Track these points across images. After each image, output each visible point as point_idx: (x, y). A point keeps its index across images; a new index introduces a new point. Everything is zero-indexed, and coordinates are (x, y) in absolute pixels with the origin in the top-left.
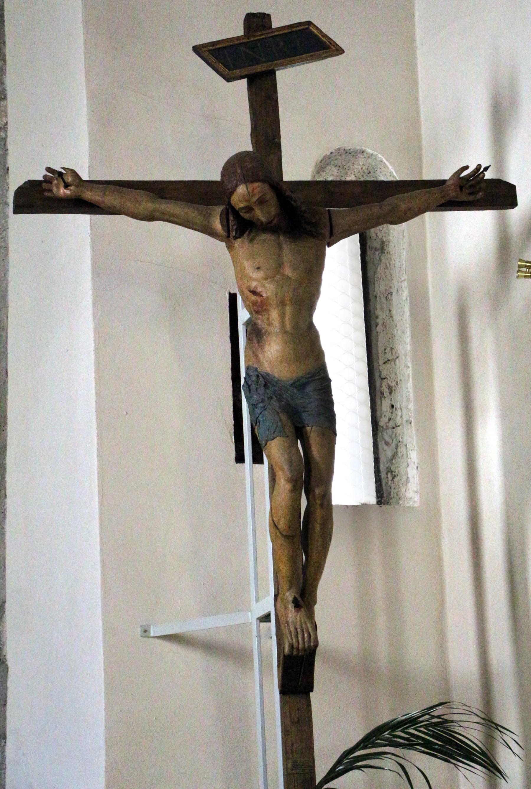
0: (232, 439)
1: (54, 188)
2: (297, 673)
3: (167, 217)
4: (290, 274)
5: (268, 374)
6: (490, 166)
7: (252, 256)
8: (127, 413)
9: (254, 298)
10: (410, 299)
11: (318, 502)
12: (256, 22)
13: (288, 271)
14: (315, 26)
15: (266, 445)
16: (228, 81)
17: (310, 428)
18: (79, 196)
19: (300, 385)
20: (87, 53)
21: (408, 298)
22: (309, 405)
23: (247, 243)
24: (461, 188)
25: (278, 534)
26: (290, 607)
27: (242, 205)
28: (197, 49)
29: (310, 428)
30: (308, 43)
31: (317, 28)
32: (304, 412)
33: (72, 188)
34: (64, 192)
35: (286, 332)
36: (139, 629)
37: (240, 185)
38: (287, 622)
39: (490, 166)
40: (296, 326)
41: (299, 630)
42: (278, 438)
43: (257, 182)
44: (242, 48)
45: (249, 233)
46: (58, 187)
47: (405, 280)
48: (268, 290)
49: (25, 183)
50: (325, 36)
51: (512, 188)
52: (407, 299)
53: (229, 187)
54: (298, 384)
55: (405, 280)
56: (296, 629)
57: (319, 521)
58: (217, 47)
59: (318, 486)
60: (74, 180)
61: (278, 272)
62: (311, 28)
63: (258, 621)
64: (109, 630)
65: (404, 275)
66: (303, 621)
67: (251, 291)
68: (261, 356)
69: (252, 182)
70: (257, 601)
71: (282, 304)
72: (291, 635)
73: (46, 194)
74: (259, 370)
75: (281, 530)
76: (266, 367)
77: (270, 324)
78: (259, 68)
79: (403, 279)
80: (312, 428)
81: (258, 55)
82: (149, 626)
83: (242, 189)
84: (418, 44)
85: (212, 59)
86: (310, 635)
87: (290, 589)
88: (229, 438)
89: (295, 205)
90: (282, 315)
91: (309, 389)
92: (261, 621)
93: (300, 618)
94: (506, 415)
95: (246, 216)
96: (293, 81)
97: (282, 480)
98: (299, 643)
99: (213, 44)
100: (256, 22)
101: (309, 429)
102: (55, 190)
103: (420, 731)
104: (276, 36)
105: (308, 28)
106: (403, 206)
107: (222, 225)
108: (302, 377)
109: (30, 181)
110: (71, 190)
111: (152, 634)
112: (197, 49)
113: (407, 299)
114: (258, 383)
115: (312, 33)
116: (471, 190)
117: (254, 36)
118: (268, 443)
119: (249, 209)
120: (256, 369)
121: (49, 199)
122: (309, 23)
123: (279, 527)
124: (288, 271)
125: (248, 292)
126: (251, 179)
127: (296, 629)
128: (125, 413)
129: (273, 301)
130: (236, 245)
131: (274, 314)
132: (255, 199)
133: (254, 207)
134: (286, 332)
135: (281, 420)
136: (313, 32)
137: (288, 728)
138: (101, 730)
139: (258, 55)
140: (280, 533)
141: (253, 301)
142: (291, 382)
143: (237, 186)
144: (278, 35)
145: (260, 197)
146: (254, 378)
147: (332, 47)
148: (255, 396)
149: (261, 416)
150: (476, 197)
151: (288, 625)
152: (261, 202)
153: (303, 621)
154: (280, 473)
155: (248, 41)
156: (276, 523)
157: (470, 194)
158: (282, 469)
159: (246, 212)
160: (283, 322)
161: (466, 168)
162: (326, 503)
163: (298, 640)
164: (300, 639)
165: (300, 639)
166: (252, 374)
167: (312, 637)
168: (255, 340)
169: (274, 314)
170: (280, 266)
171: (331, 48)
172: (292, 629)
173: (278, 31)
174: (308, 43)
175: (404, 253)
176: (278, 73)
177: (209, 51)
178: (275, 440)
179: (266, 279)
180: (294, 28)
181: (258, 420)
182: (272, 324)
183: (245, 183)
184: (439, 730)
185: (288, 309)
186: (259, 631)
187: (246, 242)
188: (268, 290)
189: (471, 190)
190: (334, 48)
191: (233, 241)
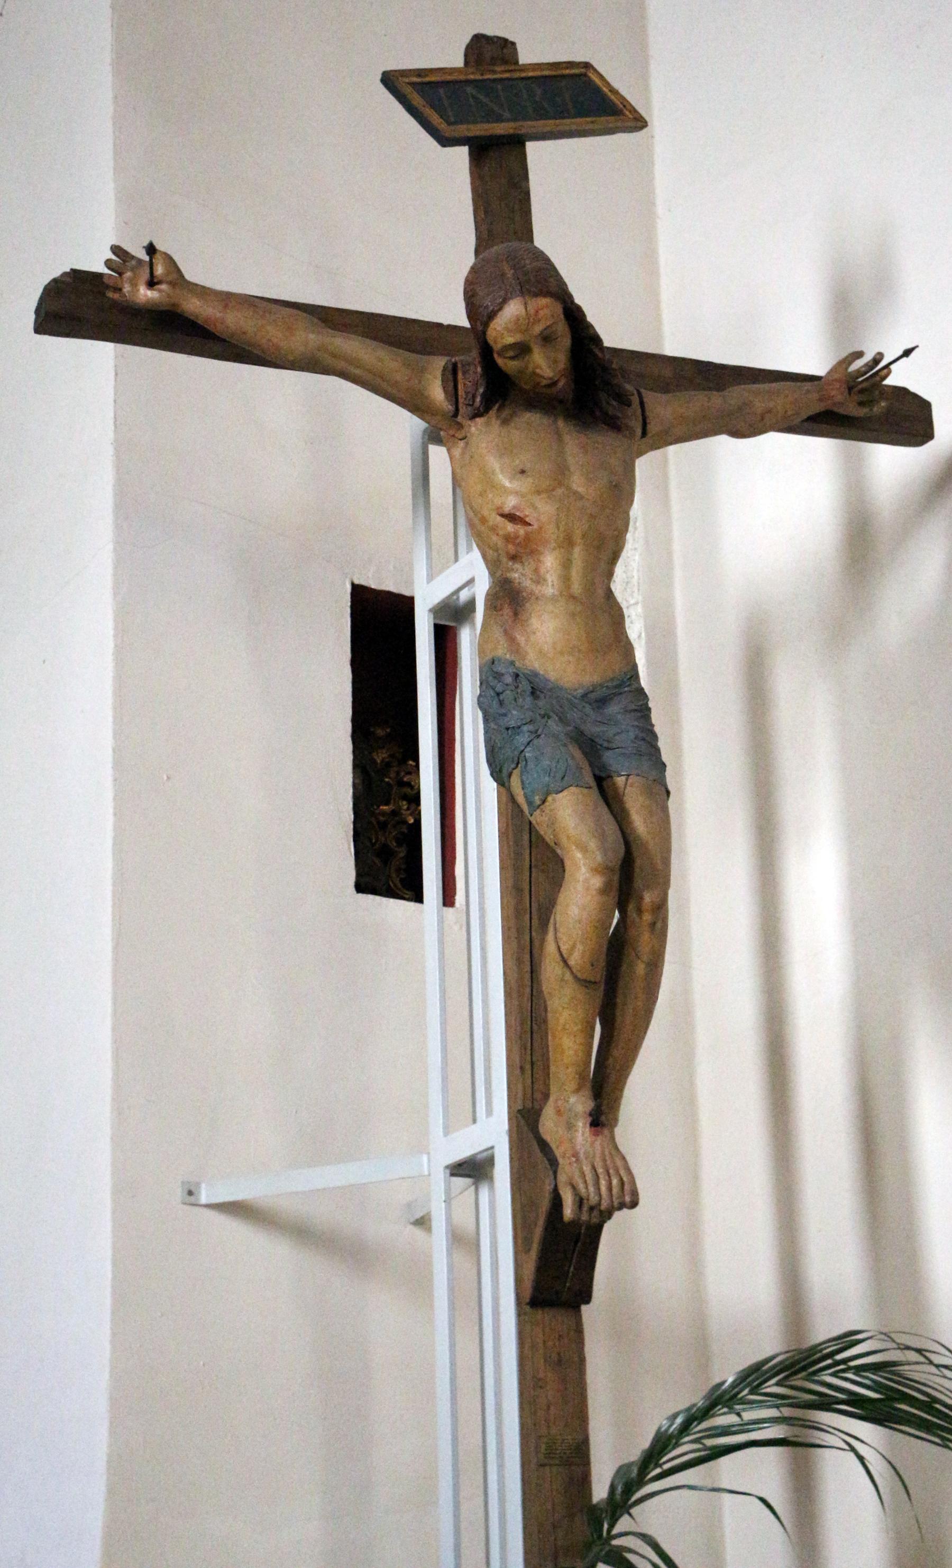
0: (349, 848)
1: (126, 286)
2: (561, 1263)
3: (341, 365)
4: (581, 490)
5: (536, 674)
6: (917, 347)
7: (505, 451)
8: (168, 778)
9: (510, 527)
10: (647, 635)
11: (647, 917)
12: (489, 51)
13: (577, 482)
14: (595, 70)
15: (544, 802)
16: (444, 146)
17: (623, 778)
18: (174, 305)
19: (598, 699)
20: (119, 121)
21: (643, 635)
22: (617, 737)
23: (496, 426)
24: (850, 389)
25: (568, 976)
26: (580, 1124)
27: (510, 340)
28: (390, 80)
29: (623, 778)
30: (585, 102)
31: (601, 77)
32: (608, 749)
33: (163, 287)
34: (146, 295)
35: (573, 597)
36: (180, 1190)
37: (511, 298)
38: (576, 1155)
39: (917, 347)
40: (590, 587)
41: (600, 1170)
42: (573, 789)
43: (545, 296)
44: (469, 90)
45: (498, 410)
46: (134, 285)
47: (637, 603)
48: (543, 512)
49: (65, 274)
50: (615, 92)
51: (924, 407)
52: (639, 637)
53: (487, 302)
54: (593, 696)
55: (637, 603)
56: (594, 1168)
57: (645, 958)
58: (427, 79)
59: (648, 887)
60: (168, 273)
61: (560, 484)
62: (590, 75)
63: (448, 1171)
64: (125, 1189)
65: (635, 595)
66: (607, 1153)
67: (502, 515)
68: (521, 639)
69: (536, 295)
70: (447, 1131)
71: (568, 542)
72: (585, 1182)
73: (110, 294)
74: (517, 664)
75: (574, 971)
76: (533, 662)
77: (539, 580)
78: (500, 129)
79: (632, 602)
80: (627, 780)
81: (499, 110)
82: (198, 1185)
83: (513, 309)
84: (660, 210)
85: (417, 100)
86: (622, 1183)
87: (577, 1090)
88: (346, 846)
89: (600, 355)
90: (566, 564)
91: (613, 709)
92: (452, 1175)
93: (603, 1147)
94: (856, 827)
95: (507, 365)
96: (553, 164)
97: (583, 870)
98: (600, 1195)
99: (420, 73)
100: (489, 51)
101: (620, 781)
102: (127, 288)
103: (846, 1379)
104: (529, 78)
105: (585, 75)
106: (759, 405)
107: (445, 391)
108: (601, 685)
109: (74, 271)
110: (160, 291)
111: (203, 1200)
112: (390, 80)
113: (639, 637)
114: (517, 687)
115: (590, 82)
116: (863, 398)
117: (494, 72)
118: (550, 799)
119: (522, 350)
120: (512, 663)
121: (114, 304)
122: (587, 65)
123: (572, 962)
124: (577, 482)
125: (499, 518)
126: (533, 289)
127: (594, 1168)
128: (165, 778)
129: (551, 532)
130: (473, 429)
131: (550, 562)
132: (538, 329)
133: (532, 345)
134: (573, 597)
135: (573, 757)
136: (594, 81)
137: (541, 1375)
138: (104, 1379)
139: (499, 110)
140: (572, 972)
141: (509, 534)
142: (580, 691)
143: (505, 301)
144: (536, 78)
145: (548, 327)
146: (509, 679)
147: (627, 113)
148: (514, 712)
149: (528, 749)
150: (871, 410)
151: (577, 1160)
152: (547, 339)
153: (607, 1153)
154: (579, 855)
155: (481, 78)
156: (564, 952)
157: (861, 404)
158: (584, 849)
159: (512, 358)
160: (566, 579)
161: (860, 354)
162: (659, 925)
163: (599, 1189)
164: (603, 1188)
165: (603, 1188)
166: (503, 671)
167: (627, 1187)
168: (507, 611)
169: (550, 562)
170: (561, 472)
171: (624, 115)
172: (587, 1169)
173: (534, 70)
174: (585, 102)
175: (637, 558)
176: (531, 147)
177: (412, 84)
178: (565, 793)
179: (539, 492)
180: (562, 69)
181: (522, 758)
182: (545, 580)
183: (522, 294)
184: (881, 1377)
185: (578, 553)
186: (448, 1191)
187: (496, 424)
188: (543, 512)
189: (863, 398)
190: (631, 116)
191: (466, 422)
